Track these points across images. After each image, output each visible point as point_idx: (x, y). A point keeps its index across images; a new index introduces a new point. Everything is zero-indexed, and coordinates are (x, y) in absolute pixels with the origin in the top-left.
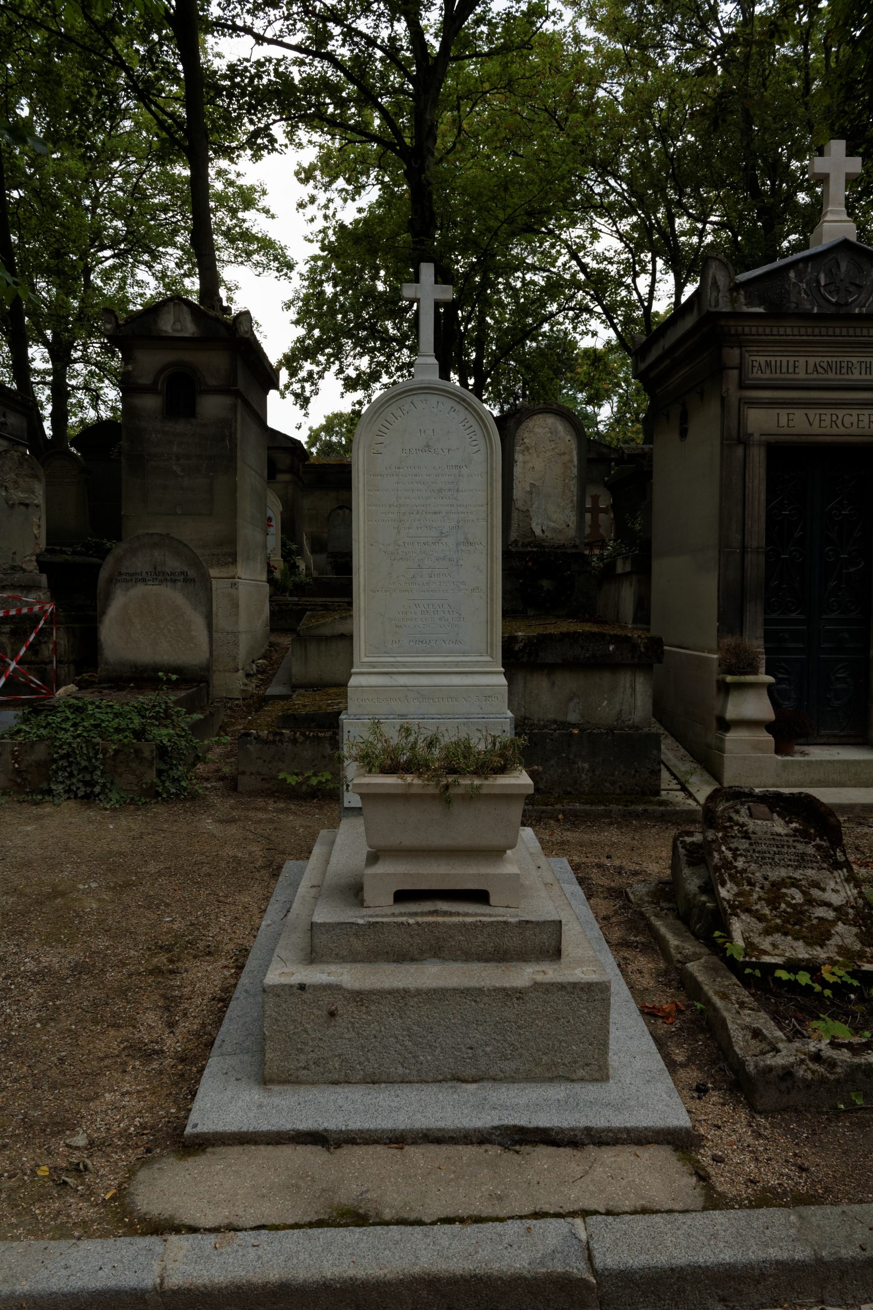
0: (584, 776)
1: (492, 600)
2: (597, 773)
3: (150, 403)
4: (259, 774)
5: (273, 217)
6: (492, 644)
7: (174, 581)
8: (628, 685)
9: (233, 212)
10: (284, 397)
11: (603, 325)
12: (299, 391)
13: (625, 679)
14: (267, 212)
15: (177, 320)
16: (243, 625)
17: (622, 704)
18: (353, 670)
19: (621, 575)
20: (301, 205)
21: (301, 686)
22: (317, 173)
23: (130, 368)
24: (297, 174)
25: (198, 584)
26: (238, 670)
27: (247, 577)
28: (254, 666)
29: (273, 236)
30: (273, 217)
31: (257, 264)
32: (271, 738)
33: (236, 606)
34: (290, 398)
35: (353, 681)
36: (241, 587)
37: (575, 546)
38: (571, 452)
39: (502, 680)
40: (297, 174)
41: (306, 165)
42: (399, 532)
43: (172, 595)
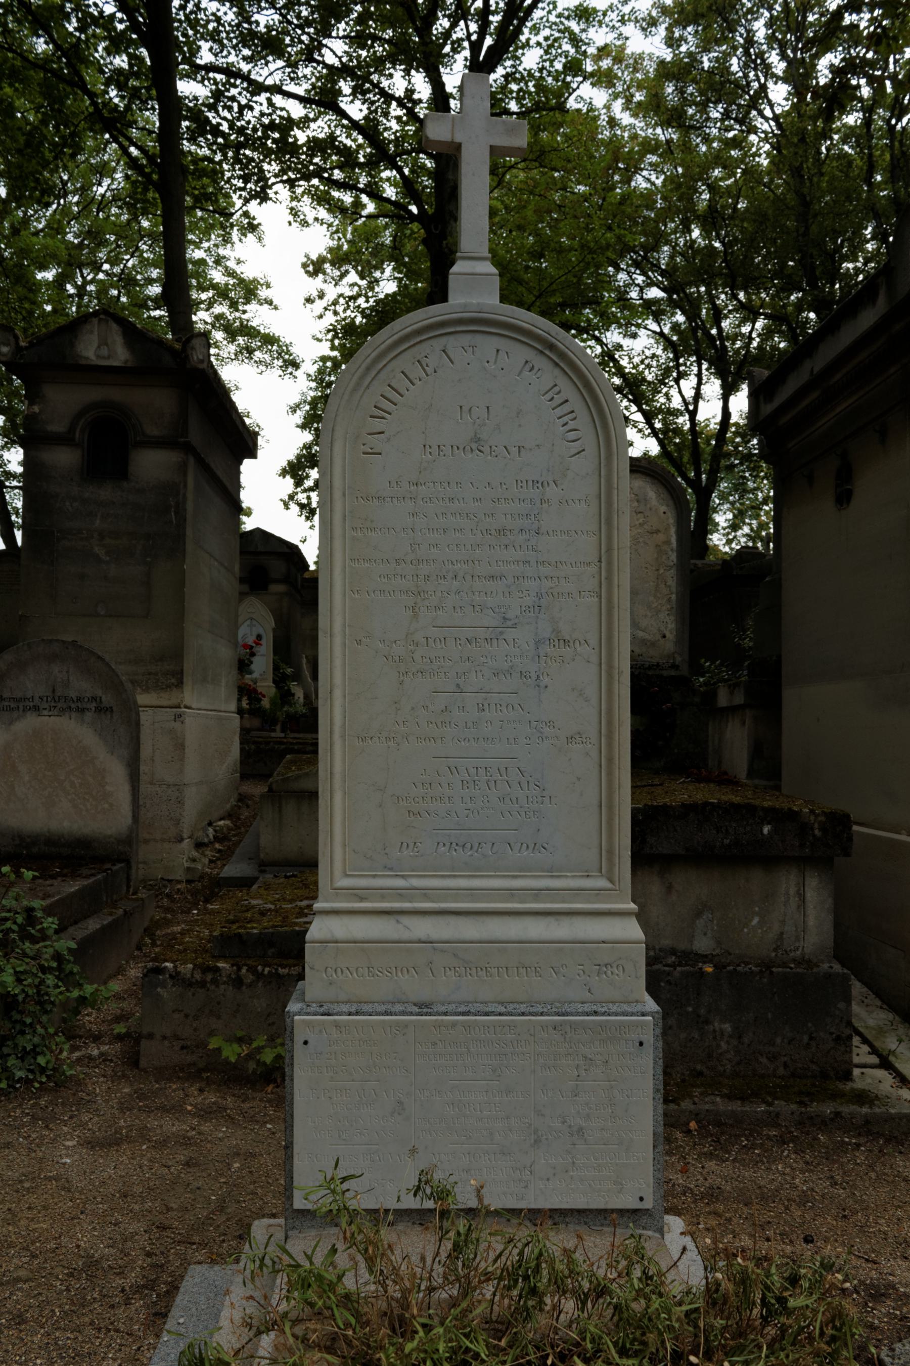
0: (724, 1046)
1: (610, 760)
2: (746, 1041)
3: (64, 458)
4: (176, 1037)
5: (276, 308)
6: (610, 852)
7: (82, 711)
8: (792, 891)
9: (234, 305)
10: (288, 508)
11: (640, 435)
12: (305, 501)
13: (787, 882)
14: (270, 303)
15: (103, 342)
16: (192, 771)
17: (783, 922)
18: (317, 906)
19: (723, 710)
20: (309, 300)
21: (274, 864)
22: (327, 266)
23: (36, 409)
24: (304, 266)
25: (117, 714)
26: (181, 840)
27: (199, 706)
28: (211, 831)
29: (275, 330)
30: (276, 308)
31: (259, 362)
32: (198, 976)
33: (181, 746)
34: (295, 508)
35: (318, 929)
36: (188, 720)
37: (674, 666)
38: (667, 529)
39: (633, 930)
40: (304, 266)
41: (314, 257)
42: (415, 616)
43: (80, 732)
